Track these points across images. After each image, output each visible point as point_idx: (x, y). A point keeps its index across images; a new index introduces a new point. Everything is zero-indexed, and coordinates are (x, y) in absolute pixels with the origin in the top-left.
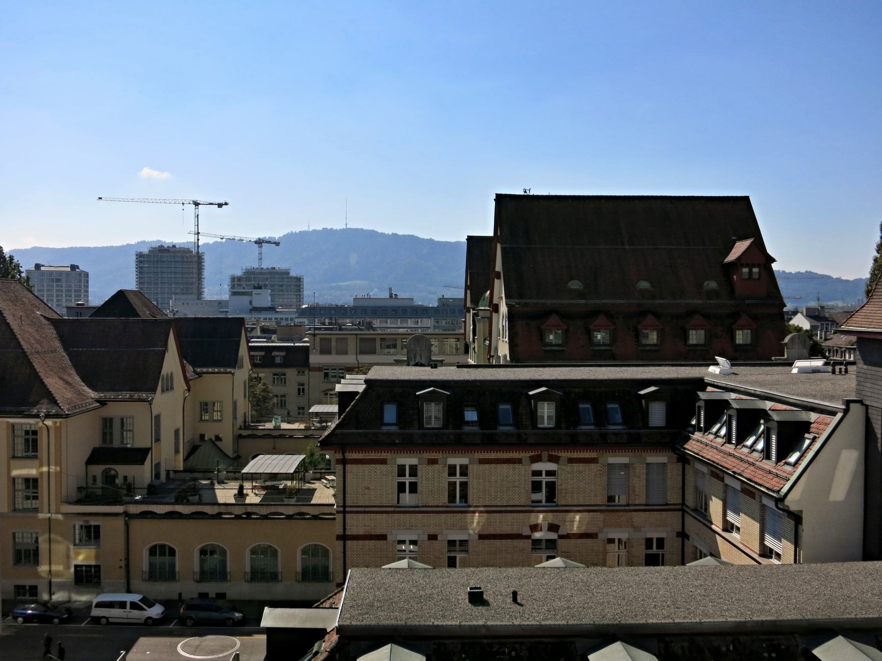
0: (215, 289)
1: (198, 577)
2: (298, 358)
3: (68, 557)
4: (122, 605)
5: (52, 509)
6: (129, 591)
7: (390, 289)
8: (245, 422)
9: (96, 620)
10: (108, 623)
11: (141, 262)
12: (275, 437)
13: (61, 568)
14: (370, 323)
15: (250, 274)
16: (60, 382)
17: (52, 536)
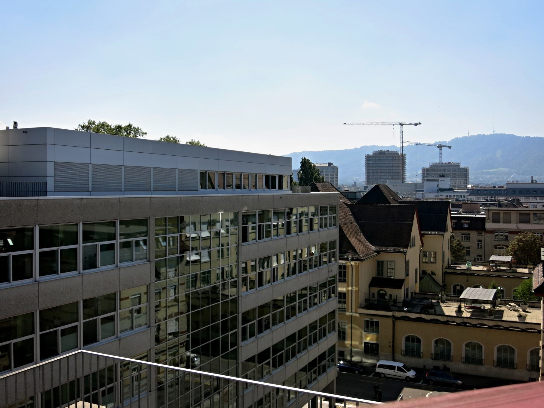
0: (413, 174)
1: (433, 356)
2: (478, 225)
3: (361, 337)
4: (393, 368)
5: (354, 311)
6: (394, 360)
7: (532, 177)
8: (448, 264)
9: (379, 374)
10: (385, 377)
11: (368, 160)
12: (468, 275)
13: (357, 343)
14: (518, 200)
15: (434, 167)
16: (357, 241)
17: (353, 325)
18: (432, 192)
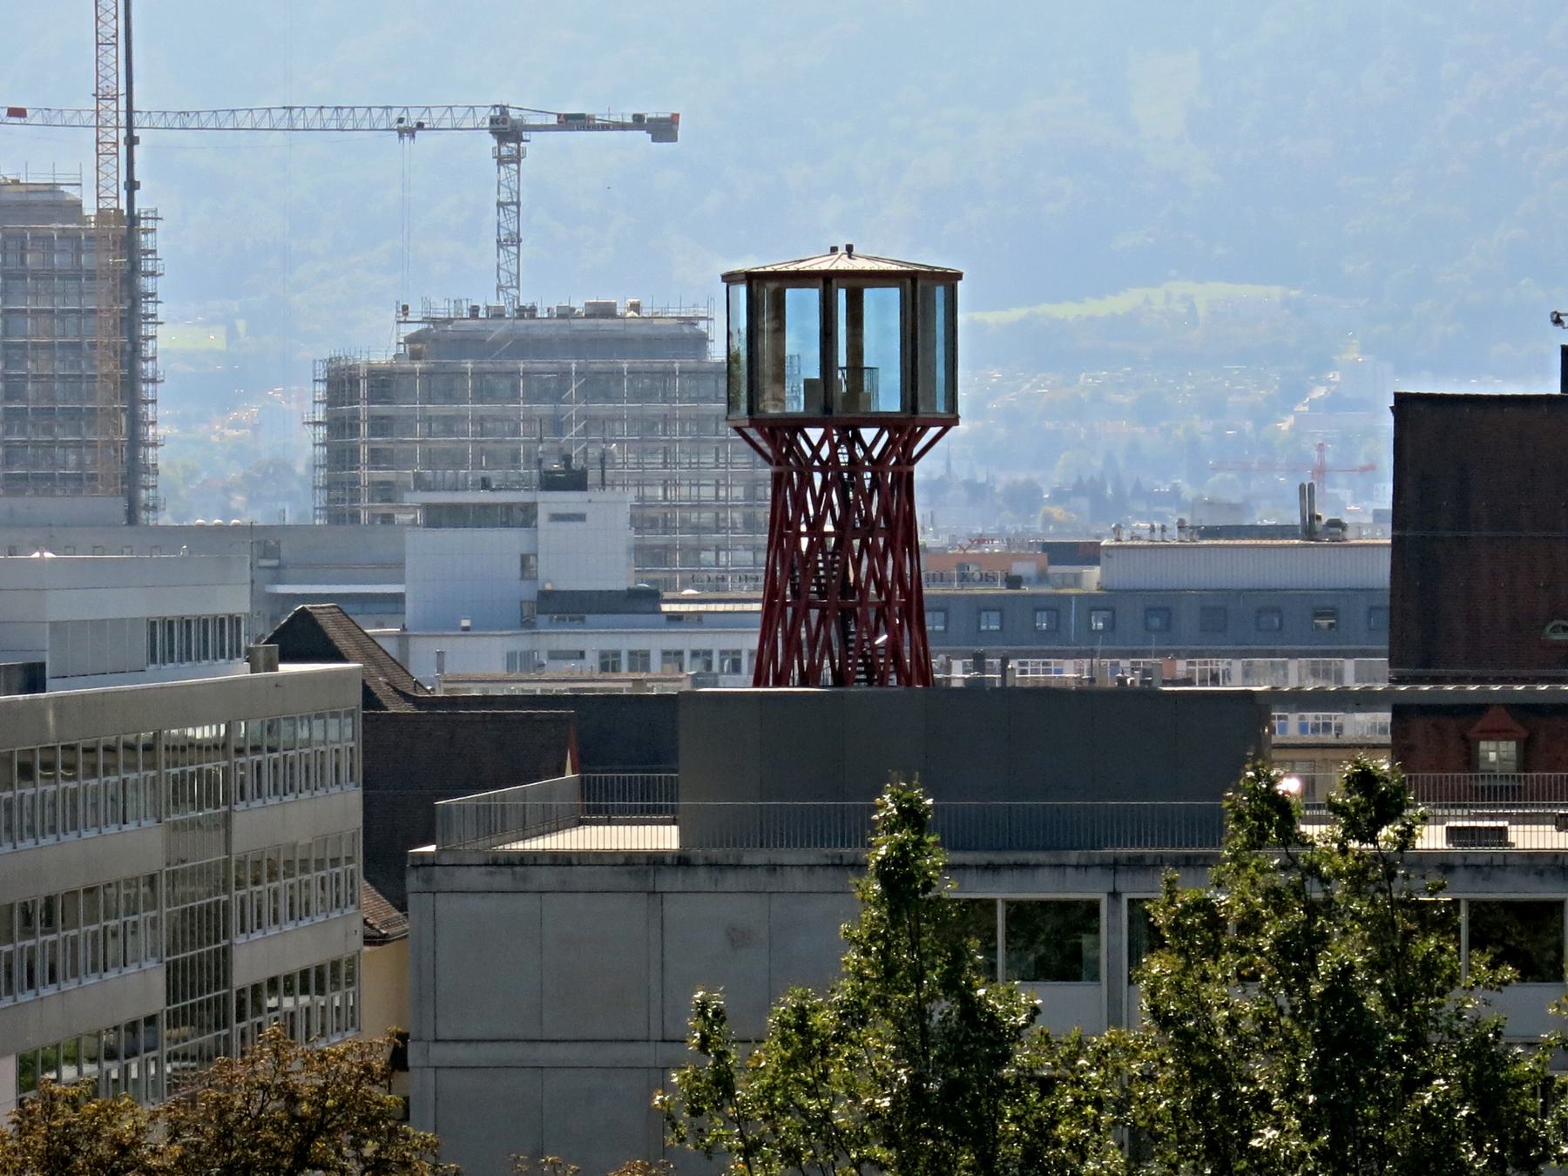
18: (485, 624)
